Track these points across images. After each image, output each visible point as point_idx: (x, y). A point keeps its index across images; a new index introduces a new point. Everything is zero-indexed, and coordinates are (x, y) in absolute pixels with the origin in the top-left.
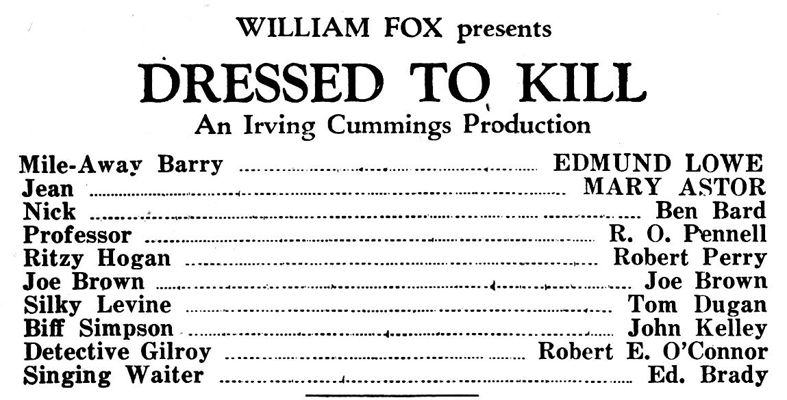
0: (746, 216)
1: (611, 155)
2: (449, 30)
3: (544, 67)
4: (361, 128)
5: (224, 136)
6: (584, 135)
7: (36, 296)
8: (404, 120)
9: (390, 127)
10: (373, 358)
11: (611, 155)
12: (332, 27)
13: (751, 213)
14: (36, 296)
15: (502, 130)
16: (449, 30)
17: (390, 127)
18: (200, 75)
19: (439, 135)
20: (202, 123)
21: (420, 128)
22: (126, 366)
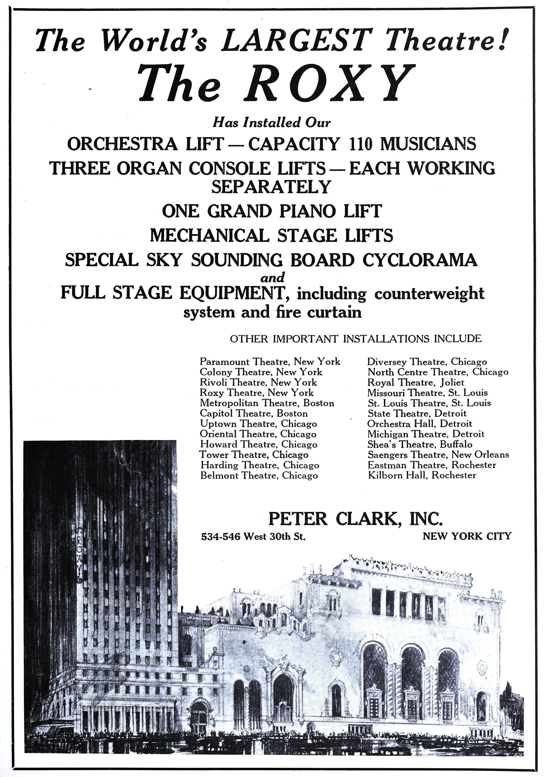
0: (229, 447)
1: (111, 30)
2: (404, 168)
3: (360, 69)
4: (241, 363)
5: (288, 540)
6: (230, 319)
7: (348, 30)
8: (478, 432)
9: (223, 363)
10: (236, 537)
11: (111, 30)
12: (371, 339)
13: (231, 446)
14: (348, 30)
15: (211, 263)
16: (404, 168)
17: (223, 363)
18: (471, 535)
19: (466, 300)
20: (169, 143)
21: (230, 466)
22: (382, 66)
